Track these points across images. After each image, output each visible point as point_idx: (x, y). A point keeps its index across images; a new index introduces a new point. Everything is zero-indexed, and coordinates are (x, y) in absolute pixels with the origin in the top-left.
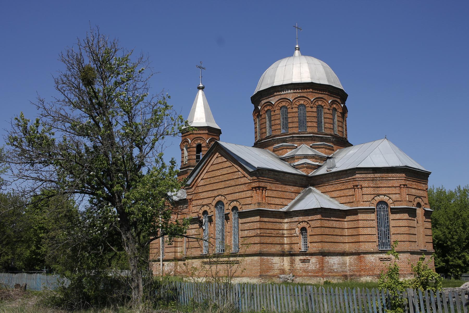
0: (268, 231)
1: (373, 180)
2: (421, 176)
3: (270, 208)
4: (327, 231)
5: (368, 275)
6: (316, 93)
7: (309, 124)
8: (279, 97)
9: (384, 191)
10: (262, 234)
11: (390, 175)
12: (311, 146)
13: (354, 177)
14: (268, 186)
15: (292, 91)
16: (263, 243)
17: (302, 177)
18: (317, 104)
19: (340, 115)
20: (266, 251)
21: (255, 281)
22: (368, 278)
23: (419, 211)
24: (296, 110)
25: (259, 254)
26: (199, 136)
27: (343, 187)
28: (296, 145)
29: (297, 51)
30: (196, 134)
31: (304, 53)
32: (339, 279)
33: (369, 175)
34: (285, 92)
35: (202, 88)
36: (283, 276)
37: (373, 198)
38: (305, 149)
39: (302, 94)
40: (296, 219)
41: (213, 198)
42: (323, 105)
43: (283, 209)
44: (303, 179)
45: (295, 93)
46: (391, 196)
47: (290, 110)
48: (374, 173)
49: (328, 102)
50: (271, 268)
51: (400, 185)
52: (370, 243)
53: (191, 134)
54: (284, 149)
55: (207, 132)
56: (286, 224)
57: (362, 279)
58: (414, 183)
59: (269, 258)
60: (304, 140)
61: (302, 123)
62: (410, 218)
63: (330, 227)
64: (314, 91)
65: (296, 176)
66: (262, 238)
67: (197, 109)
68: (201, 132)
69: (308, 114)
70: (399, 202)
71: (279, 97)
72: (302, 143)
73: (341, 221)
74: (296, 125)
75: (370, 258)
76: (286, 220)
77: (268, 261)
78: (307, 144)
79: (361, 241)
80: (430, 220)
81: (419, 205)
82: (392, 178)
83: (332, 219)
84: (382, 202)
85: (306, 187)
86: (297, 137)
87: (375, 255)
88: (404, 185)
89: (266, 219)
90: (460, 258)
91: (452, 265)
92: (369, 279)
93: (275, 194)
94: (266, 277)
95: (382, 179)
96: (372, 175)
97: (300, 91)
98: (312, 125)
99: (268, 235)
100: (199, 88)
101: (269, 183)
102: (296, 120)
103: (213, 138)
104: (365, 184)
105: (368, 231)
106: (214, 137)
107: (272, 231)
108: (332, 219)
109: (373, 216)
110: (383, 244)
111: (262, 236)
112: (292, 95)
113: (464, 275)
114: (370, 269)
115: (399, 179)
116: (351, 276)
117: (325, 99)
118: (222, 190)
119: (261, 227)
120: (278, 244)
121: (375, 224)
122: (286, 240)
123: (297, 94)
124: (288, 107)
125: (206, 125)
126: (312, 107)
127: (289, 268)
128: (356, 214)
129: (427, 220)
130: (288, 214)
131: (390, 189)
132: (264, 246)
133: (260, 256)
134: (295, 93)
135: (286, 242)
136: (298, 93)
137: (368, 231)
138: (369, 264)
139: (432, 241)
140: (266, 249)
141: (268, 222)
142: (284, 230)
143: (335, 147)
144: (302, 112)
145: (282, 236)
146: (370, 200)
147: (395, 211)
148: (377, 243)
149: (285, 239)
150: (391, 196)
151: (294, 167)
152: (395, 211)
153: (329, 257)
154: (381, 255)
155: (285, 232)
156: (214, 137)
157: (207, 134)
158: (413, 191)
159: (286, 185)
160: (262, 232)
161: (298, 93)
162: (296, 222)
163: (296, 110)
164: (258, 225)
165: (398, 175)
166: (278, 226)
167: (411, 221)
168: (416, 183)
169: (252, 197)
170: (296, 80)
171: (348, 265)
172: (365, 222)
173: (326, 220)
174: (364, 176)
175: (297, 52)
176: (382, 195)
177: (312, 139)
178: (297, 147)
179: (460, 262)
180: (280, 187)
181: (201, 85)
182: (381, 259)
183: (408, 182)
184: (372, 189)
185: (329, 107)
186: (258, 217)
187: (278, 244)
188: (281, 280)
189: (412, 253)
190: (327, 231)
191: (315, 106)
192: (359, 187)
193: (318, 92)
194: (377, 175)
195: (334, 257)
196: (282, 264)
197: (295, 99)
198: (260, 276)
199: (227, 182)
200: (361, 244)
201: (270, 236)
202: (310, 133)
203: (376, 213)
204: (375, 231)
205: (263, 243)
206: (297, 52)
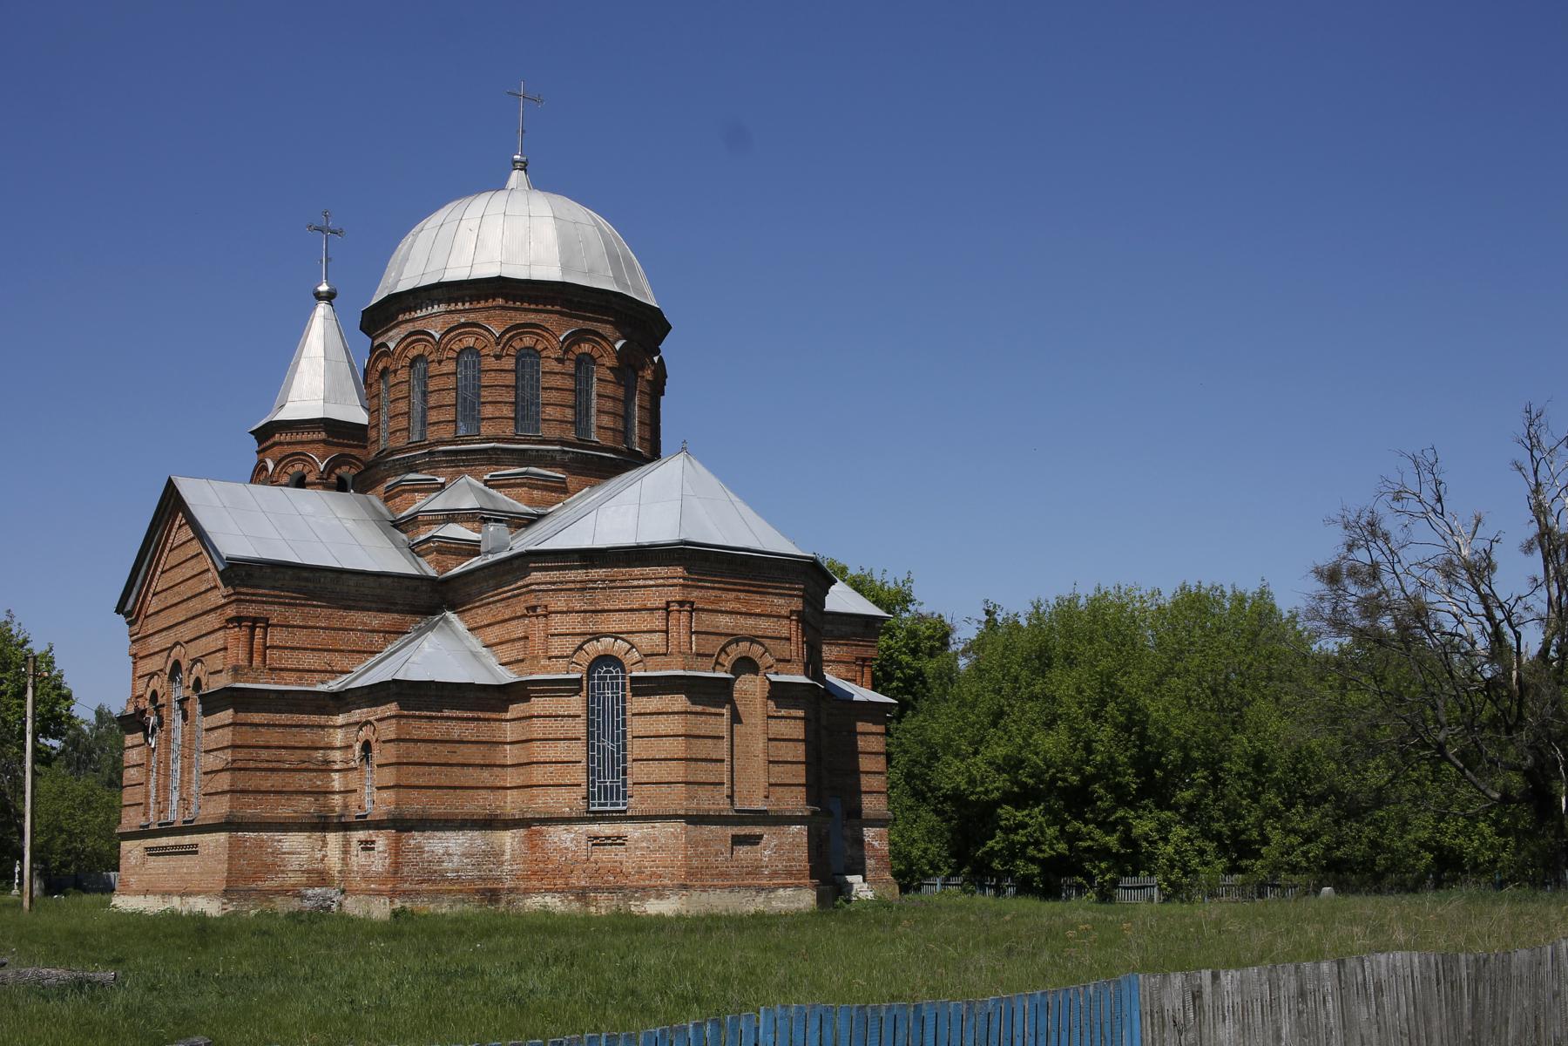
0: (264, 754)
3: (281, 681)
5: (547, 891)
7: (488, 411)
8: (409, 327)
9: (614, 623)
10: (240, 764)
11: (637, 571)
12: (486, 482)
13: (528, 580)
14: (275, 613)
15: (443, 307)
16: (242, 792)
17: (418, 583)
18: (517, 344)
19: (610, 376)
20: (253, 815)
22: (548, 899)
23: (750, 688)
24: (449, 367)
25: (227, 823)
26: (299, 449)
28: (441, 480)
29: (515, 173)
30: (289, 444)
31: (542, 182)
33: (572, 575)
34: (424, 312)
35: (329, 297)
36: (318, 890)
37: (580, 648)
38: (465, 492)
39: (472, 317)
40: (357, 715)
41: (723, 641)
43: (331, 683)
45: (451, 312)
46: (635, 639)
48: (586, 567)
49: (556, 337)
51: (668, 603)
53: (275, 444)
54: (404, 491)
55: (323, 435)
56: (339, 732)
57: (528, 902)
58: (732, 595)
59: (264, 835)
61: (468, 408)
62: (699, 708)
64: (511, 304)
68: (305, 437)
69: (485, 381)
70: (659, 659)
71: (409, 327)
72: (460, 473)
74: (448, 415)
75: (563, 838)
76: (340, 719)
77: (260, 845)
78: (477, 476)
79: (534, 782)
80: (801, 713)
82: (641, 583)
83: (447, 713)
85: (434, 614)
86: (445, 452)
87: (576, 828)
88: (681, 603)
89: (257, 718)
91: (1089, 849)
92: (555, 903)
93: (300, 638)
94: (246, 894)
95: (611, 585)
96: (580, 575)
99: (265, 765)
100: (319, 297)
102: (449, 398)
104: (558, 602)
105: (559, 751)
107: (283, 752)
108: (447, 713)
109: (576, 704)
111: (240, 769)
112: (440, 320)
113: (1127, 881)
114: (559, 872)
115: (664, 584)
116: (511, 891)
117: (546, 330)
118: (181, 628)
120: (304, 793)
121: (580, 728)
122: (337, 782)
124: (484, 352)
125: (318, 414)
127: (338, 867)
129: (783, 712)
130: (341, 701)
131: (635, 616)
132: (249, 799)
134: (451, 312)
137: (559, 751)
139: (803, 781)
141: (268, 725)
143: (572, 481)
147: (645, 687)
148: (582, 791)
149: (336, 776)
150: (635, 639)
151: (416, 550)
152: (645, 687)
153: (427, 834)
154: (595, 828)
155: (337, 755)
157: (324, 441)
158: (724, 622)
159: (348, 608)
160: (239, 756)
163: (449, 367)
164: (675, 725)
165: (663, 571)
166: (308, 737)
167: (704, 718)
168: (742, 595)
169: (225, 649)
170: (458, 272)
172: (550, 722)
173: (420, 717)
174: (554, 575)
175: (517, 177)
177: (492, 457)
178: (443, 485)
179: (1112, 841)
180: (322, 615)
181: (324, 288)
182: (596, 841)
183: (696, 593)
184: (578, 618)
185: (560, 354)
186: (231, 711)
187: (304, 793)
188: (307, 904)
189: (695, 820)
190: (421, 752)
191: (512, 351)
192: (539, 610)
195: (448, 834)
196: (319, 855)
197: (447, 332)
199: (191, 604)
200: (535, 791)
201: (273, 770)
202: (488, 440)
203: (584, 693)
204: (578, 751)
205: (242, 792)
206: (517, 177)
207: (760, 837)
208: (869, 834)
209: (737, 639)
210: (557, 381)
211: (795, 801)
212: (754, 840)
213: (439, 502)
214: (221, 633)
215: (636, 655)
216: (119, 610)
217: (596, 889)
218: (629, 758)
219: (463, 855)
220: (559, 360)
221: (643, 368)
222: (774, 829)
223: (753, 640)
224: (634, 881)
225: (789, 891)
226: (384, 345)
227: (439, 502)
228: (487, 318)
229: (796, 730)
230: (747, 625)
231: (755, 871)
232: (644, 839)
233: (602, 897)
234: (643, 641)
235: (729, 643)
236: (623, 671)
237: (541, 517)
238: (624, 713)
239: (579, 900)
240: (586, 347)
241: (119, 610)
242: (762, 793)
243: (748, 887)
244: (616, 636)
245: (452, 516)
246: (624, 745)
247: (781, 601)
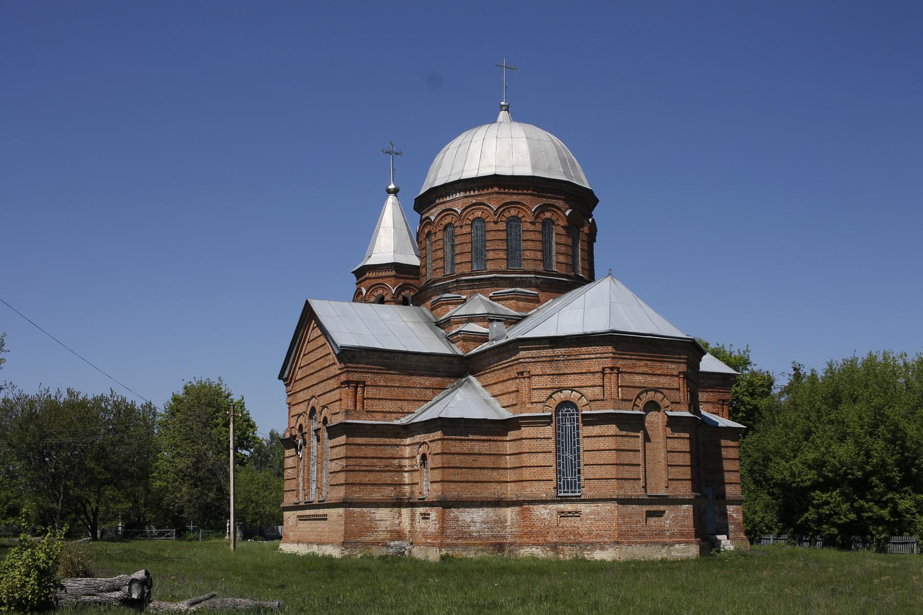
0: (364, 462)
1: (551, 360)
2: (692, 350)
4: (456, 461)
5: (533, 544)
6: (505, 193)
7: (491, 255)
8: (443, 207)
9: (571, 381)
10: (350, 468)
11: (584, 349)
12: (490, 298)
13: (518, 356)
14: (369, 378)
15: (462, 194)
16: (352, 484)
17: (450, 359)
18: (507, 214)
19: (563, 232)
21: (334, 552)
23: (655, 420)
26: (380, 281)
27: (506, 377)
28: (464, 297)
31: (518, 117)
32: (482, 550)
33: (544, 352)
34: (451, 198)
35: (395, 192)
37: (551, 397)
40: (418, 438)
42: (520, 216)
44: (450, 363)
45: (467, 197)
46: (584, 391)
47: (458, 231)
48: (550, 348)
49: (530, 209)
50: (370, 529)
51: (603, 369)
52: (542, 483)
54: (442, 304)
55: (394, 273)
56: (408, 448)
57: (522, 551)
58: (643, 363)
59: (365, 510)
60: (479, 287)
61: (479, 253)
62: (624, 433)
63: (465, 454)
64: (502, 190)
65: (432, 358)
66: (350, 474)
67: (382, 232)
69: (489, 237)
70: (599, 403)
71: (443, 207)
72: (475, 293)
73: (495, 441)
74: (467, 258)
75: (541, 511)
76: (408, 441)
77: (363, 515)
79: (524, 478)
80: (687, 435)
81: (652, 406)
82: (587, 356)
83: (471, 437)
84: (566, 404)
87: (550, 506)
88: (612, 369)
89: (360, 440)
90: (884, 505)
91: (869, 518)
92: (538, 552)
93: (383, 393)
95: (568, 358)
96: (550, 352)
97: (476, 193)
98: (496, 257)
99: (365, 468)
100: (389, 192)
101: (372, 373)
102: (467, 248)
103: (405, 284)
104: (537, 369)
106: (408, 281)
107: (375, 460)
108: (471, 437)
109: (549, 431)
110: (569, 485)
111: (350, 471)
112: (461, 202)
113: (895, 539)
114: (540, 533)
117: (524, 205)
119: (350, 455)
120: (388, 485)
121: (551, 445)
123: (470, 199)
126: (496, 223)
128: (519, 428)
129: (676, 435)
131: (583, 377)
133: (345, 507)
134: (467, 197)
135: (407, 480)
136: (472, 196)
138: (538, 524)
139: (689, 477)
140: (359, 494)
141: (366, 445)
142: (404, 458)
143: (542, 295)
144: (479, 232)
145: (400, 470)
146: (544, 399)
147: (590, 420)
148: (554, 484)
149: (406, 475)
150: (584, 391)
151: (450, 339)
152: (590, 420)
153: (461, 510)
154: (562, 507)
155: (406, 462)
156: (408, 281)
157: (394, 276)
158: (638, 380)
159: (411, 375)
160: (350, 463)
161: (472, 196)
162: (418, 443)
163: (468, 229)
164: (609, 443)
165: (600, 349)
166: (389, 451)
168: (649, 363)
169: (341, 400)
170: (470, 172)
171: (509, 523)
173: (452, 439)
174: (534, 353)
175: (503, 115)
176: (566, 389)
177: (494, 283)
178: (465, 300)
179: (885, 513)
180: (396, 379)
181: (392, 186)
183: (620, 362)
184: (549, 378)
185: (532, 219)
187: (388, 485)
190: (456, 461)
191: (504, 219)
192: (525, 374)
193: (511, 191)
194: (559, 351)
195: (473, 509)
196: (397, 522)
198: (343, 544)
200: (525, 484)
201: (369, 471)
202: (491, 272)
203: (553, 425)
204: (551, 460)
205: (352, 484)
206: (503, 115)
207: (664, 512)
208: (730, 509)
209: (647, 390)
210: (531, 236)
211: (685, 490)
212: (660, 514)
213: (463, 310)
214: (338, 390)
215: (584, 401)
217: (563, 544)
219: (483, 522)
220: (532, 223)
221: (582, 226)
222: (672, 507)
223: (656, 390)
225: (682, 546)
226: (428, 218)
227: (463, 310)
228: (488, 200)
229: (685, 445)
230: (652, 381)
231: (661, 533)
232: (592, 513)
233: (567, 548)
235: (642, 393)
236: (577, 410)
237: (524, 317)
238: (578, 436)
240: (548, 215)
241: (280, 377)
242: (664, 484)
243: (656, 543)
244: (572, 389)
245: (471, 319)
247: (673, 366)
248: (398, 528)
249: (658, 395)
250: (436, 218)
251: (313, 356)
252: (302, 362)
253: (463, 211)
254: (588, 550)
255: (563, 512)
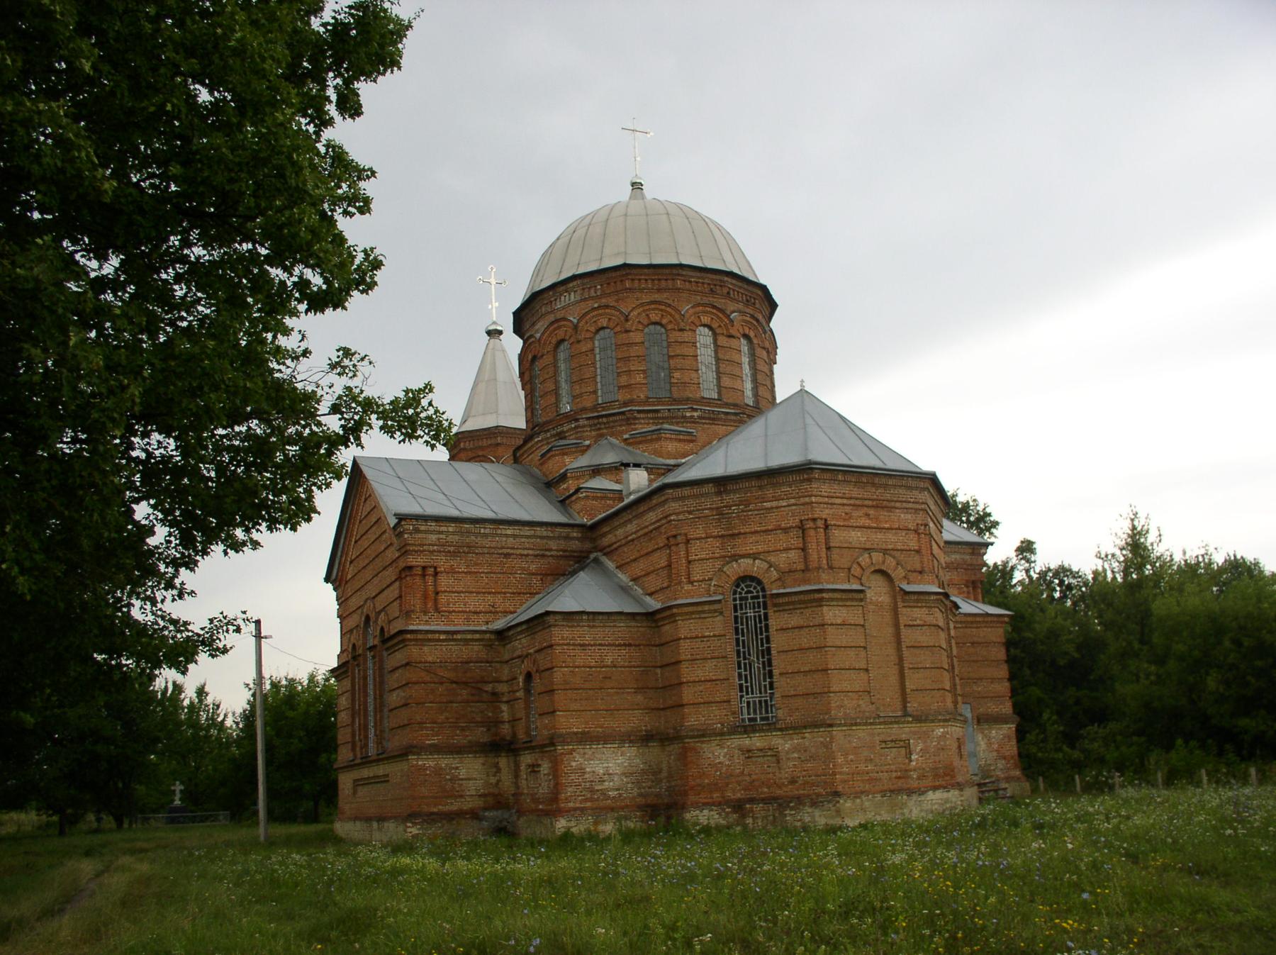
5: (705, 804)
28: (587, 443)
58: (861, 512)
71: (552, 318)
72: (602, 436)
117: (670, 306)
162: (519, 657)
168: (872, 512)
178: (589, 446)
213: (584, 461)
214: (397, 584)
215: (774, 575)
216: (327, 580)
217: (752, 800)
218: (776, 672)
219: (624, 774)
223: (885, 552)
224: (789, 790)
226: (531, 336)
227: (584, 461)
228: (617, 301)
232: (795, 749)
233: (758, 808)
234: (782, 559)
236: (763, 590)
237: (678, 466)
238: (767, 630)
239: (735, 811)
241: (327, 580)
244: (755, 556)
245: (596, 471)
246: (768, 637)
248: (496, 791)
249: (890, 560)
250: (543, 334)
251: (365, 543)
252: (353, 553)
253: (579, 321)
254: (792, 809)
255: (749, 751)
